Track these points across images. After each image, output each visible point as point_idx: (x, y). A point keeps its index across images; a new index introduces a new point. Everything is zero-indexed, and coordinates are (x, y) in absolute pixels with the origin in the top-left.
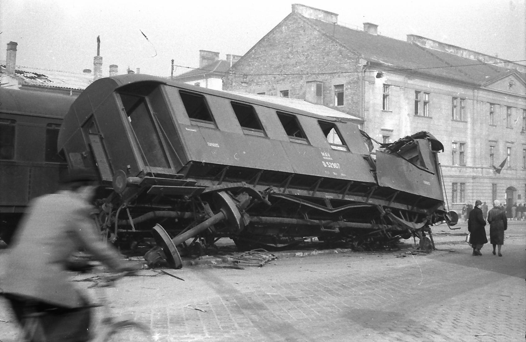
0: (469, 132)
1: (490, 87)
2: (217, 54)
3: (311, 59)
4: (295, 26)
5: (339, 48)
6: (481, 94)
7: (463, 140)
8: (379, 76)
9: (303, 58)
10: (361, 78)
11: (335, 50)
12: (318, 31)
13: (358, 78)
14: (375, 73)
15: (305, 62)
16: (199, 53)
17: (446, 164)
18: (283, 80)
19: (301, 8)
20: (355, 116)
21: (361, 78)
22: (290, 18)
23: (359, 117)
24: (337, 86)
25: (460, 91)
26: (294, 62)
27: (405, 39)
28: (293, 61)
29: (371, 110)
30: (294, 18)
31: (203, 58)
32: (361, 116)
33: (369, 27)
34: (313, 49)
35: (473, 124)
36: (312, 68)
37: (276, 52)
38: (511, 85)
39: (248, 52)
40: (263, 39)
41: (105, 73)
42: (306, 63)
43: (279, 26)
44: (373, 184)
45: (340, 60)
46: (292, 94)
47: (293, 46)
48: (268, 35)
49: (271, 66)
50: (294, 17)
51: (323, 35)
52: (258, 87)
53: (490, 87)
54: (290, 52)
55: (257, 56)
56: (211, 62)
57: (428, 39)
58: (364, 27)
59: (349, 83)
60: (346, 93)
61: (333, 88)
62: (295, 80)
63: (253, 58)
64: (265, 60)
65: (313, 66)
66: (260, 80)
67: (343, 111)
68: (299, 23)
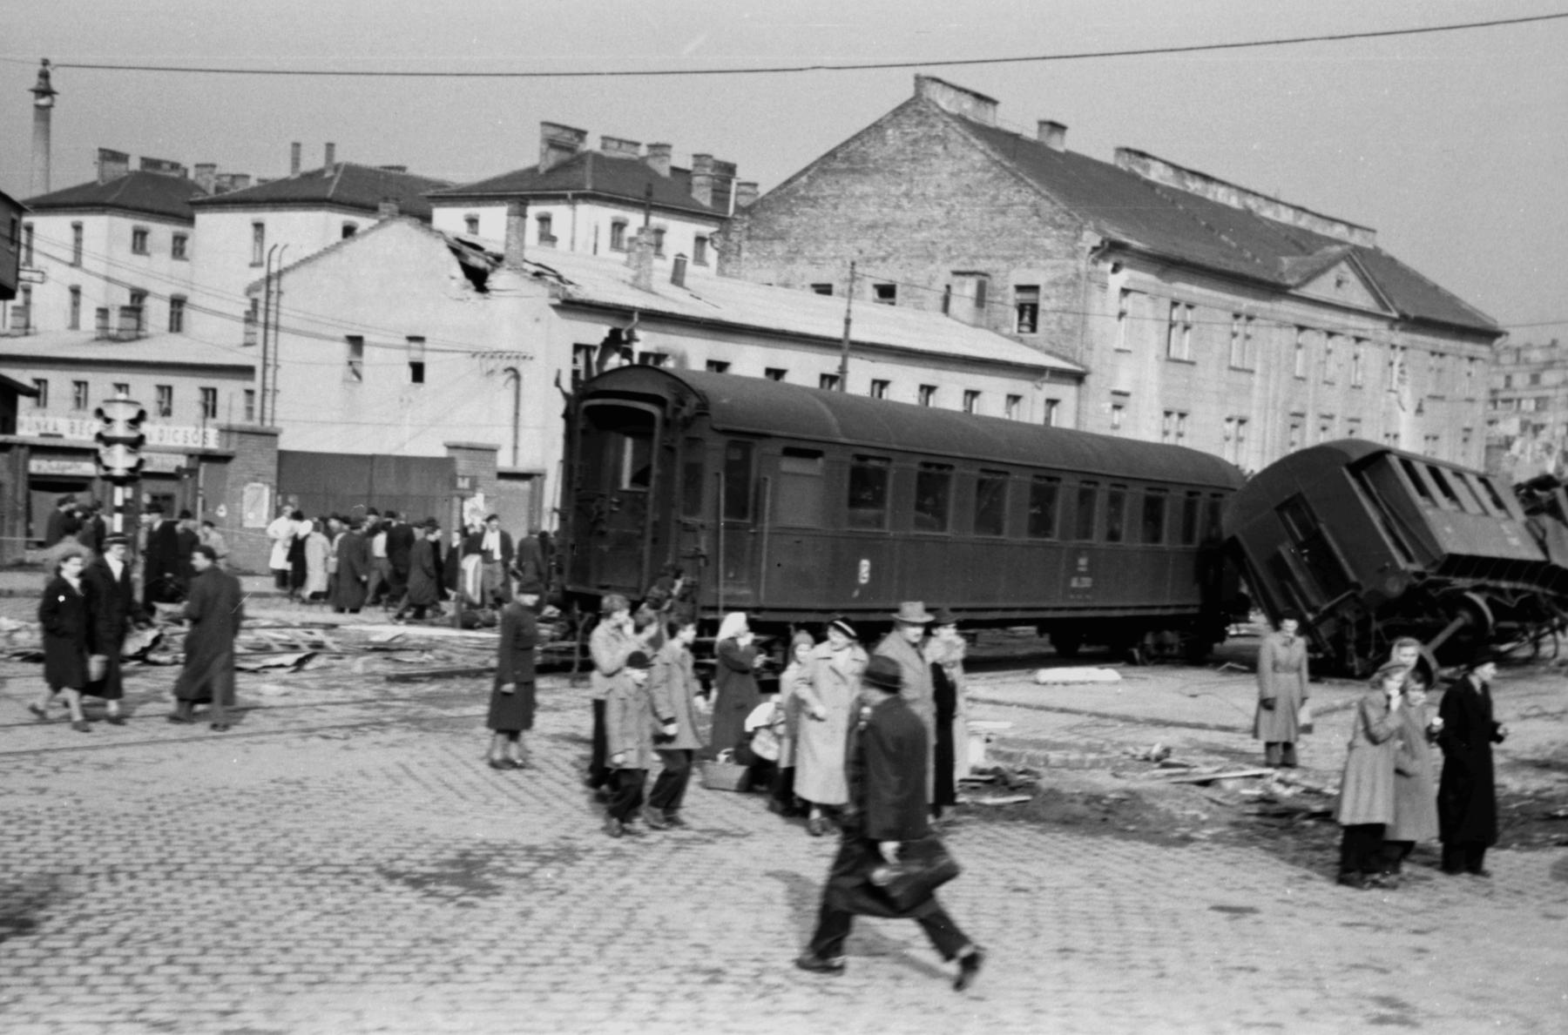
0: (1256, 393)
1: (1310, 291)
2: (581, 134)
3: (959, 218)
4: (920, 131)
5: (1032, 199)
6: (1287, 309)
7: (1244, 413)
8: (1115, 270)
9: (938, 213)
10: (1084, 276)
11: (1024, 203)
12: (983, 152)
13: (1078, 276)
14: (1110, 266)
15: (944, 223)
16: (538, 129)
17: (158, 302)
18: (884, 259)
19: (936, 87)
20: (1065, 359)
21: (1084, 276)
22: (909, 110)
23: (1076, 363)
24: (1020, 288)
25: (1246, 303)
26: (915, 221)
27: (1108, 157)
28: (909, 216)
29: (1097, 347)
30: (920, 113)
31: (552, 144)
32: (1077, 359)
33: (1051, 132)
34: (968, 194)
35: (1266, 377)
36: (962, 239)
37: (868, 189)
38: (1339, 283)
39: (789, 181)
40: (832, 154)
41: (1311, 438)
42: (945, 227)
43: (877, 127)
44: (1537, 564)
45: (1035, 229)
46: (905, 294)
47: (912, 181)
48: (847, 143)
49: (851, 221)
50: (920, 107)
51: (995, 163)
52: (813, 268)
53: (1310, 291)
54: (907, 195)
55: (812, 194)
56: (566, 156)
57: (1155, 158)
58: (1040, 130)
59: (1054, 284)
60: (1044, 305)
61: (1011, 290)
62: (915, 262)
63: (803, 198)
64: (835, 207)
65: (964, 233)
66: (819, 254)
67: (1035, 347)
68: (933, 126)
